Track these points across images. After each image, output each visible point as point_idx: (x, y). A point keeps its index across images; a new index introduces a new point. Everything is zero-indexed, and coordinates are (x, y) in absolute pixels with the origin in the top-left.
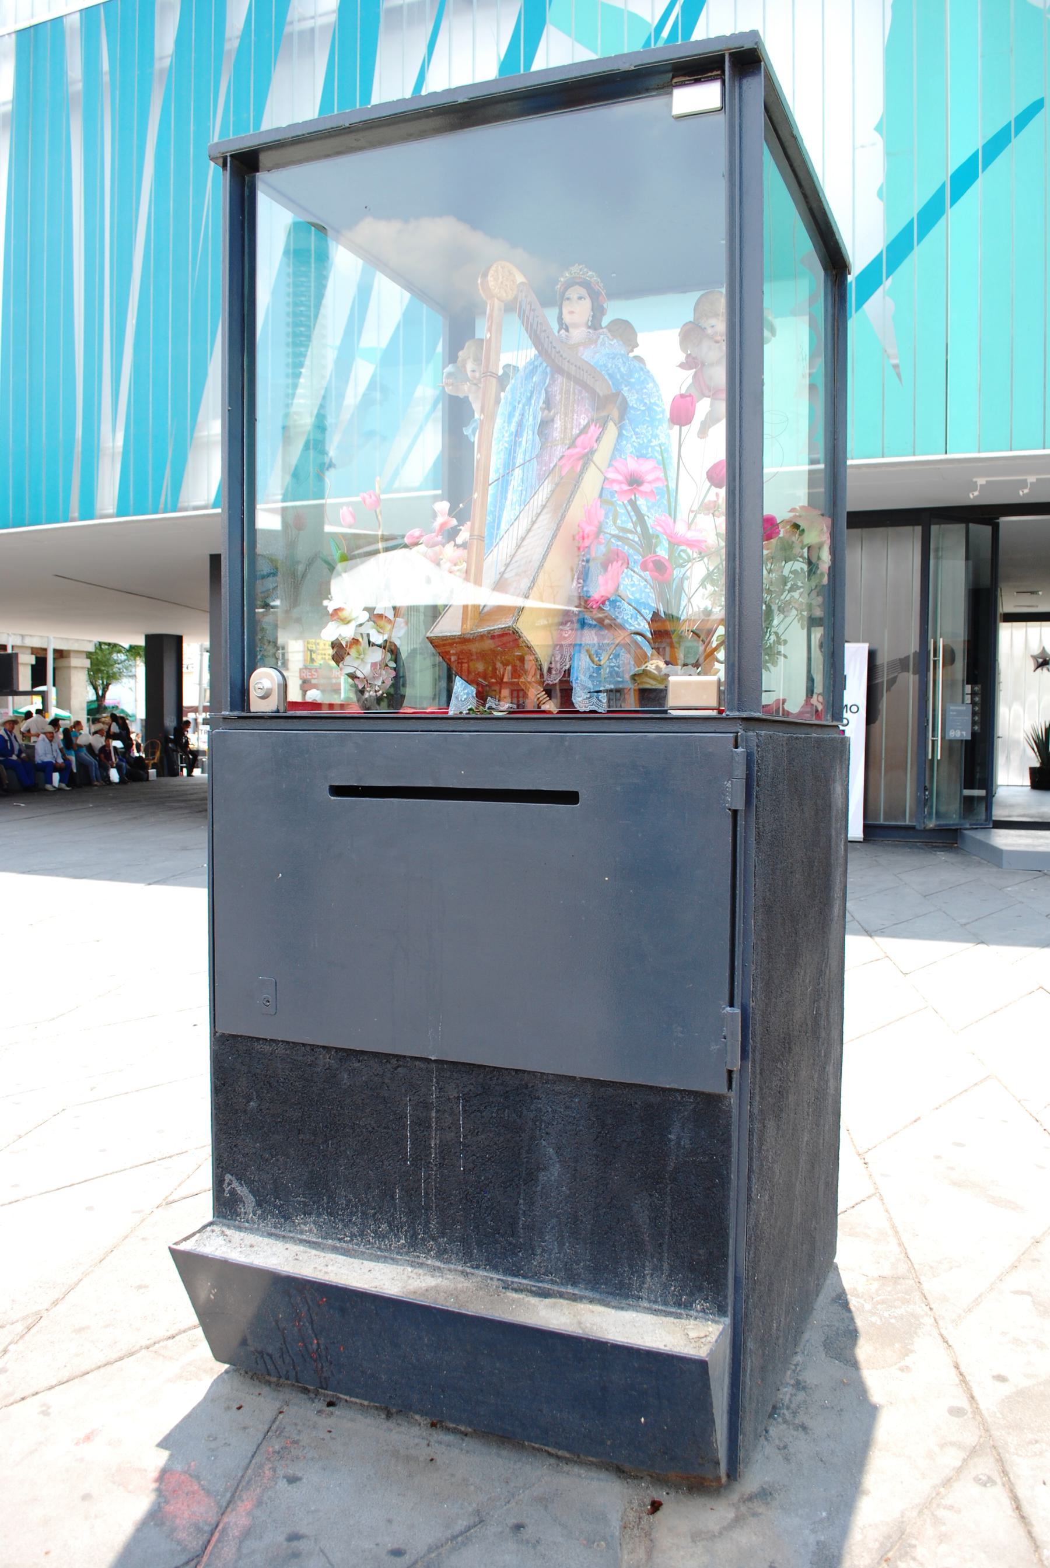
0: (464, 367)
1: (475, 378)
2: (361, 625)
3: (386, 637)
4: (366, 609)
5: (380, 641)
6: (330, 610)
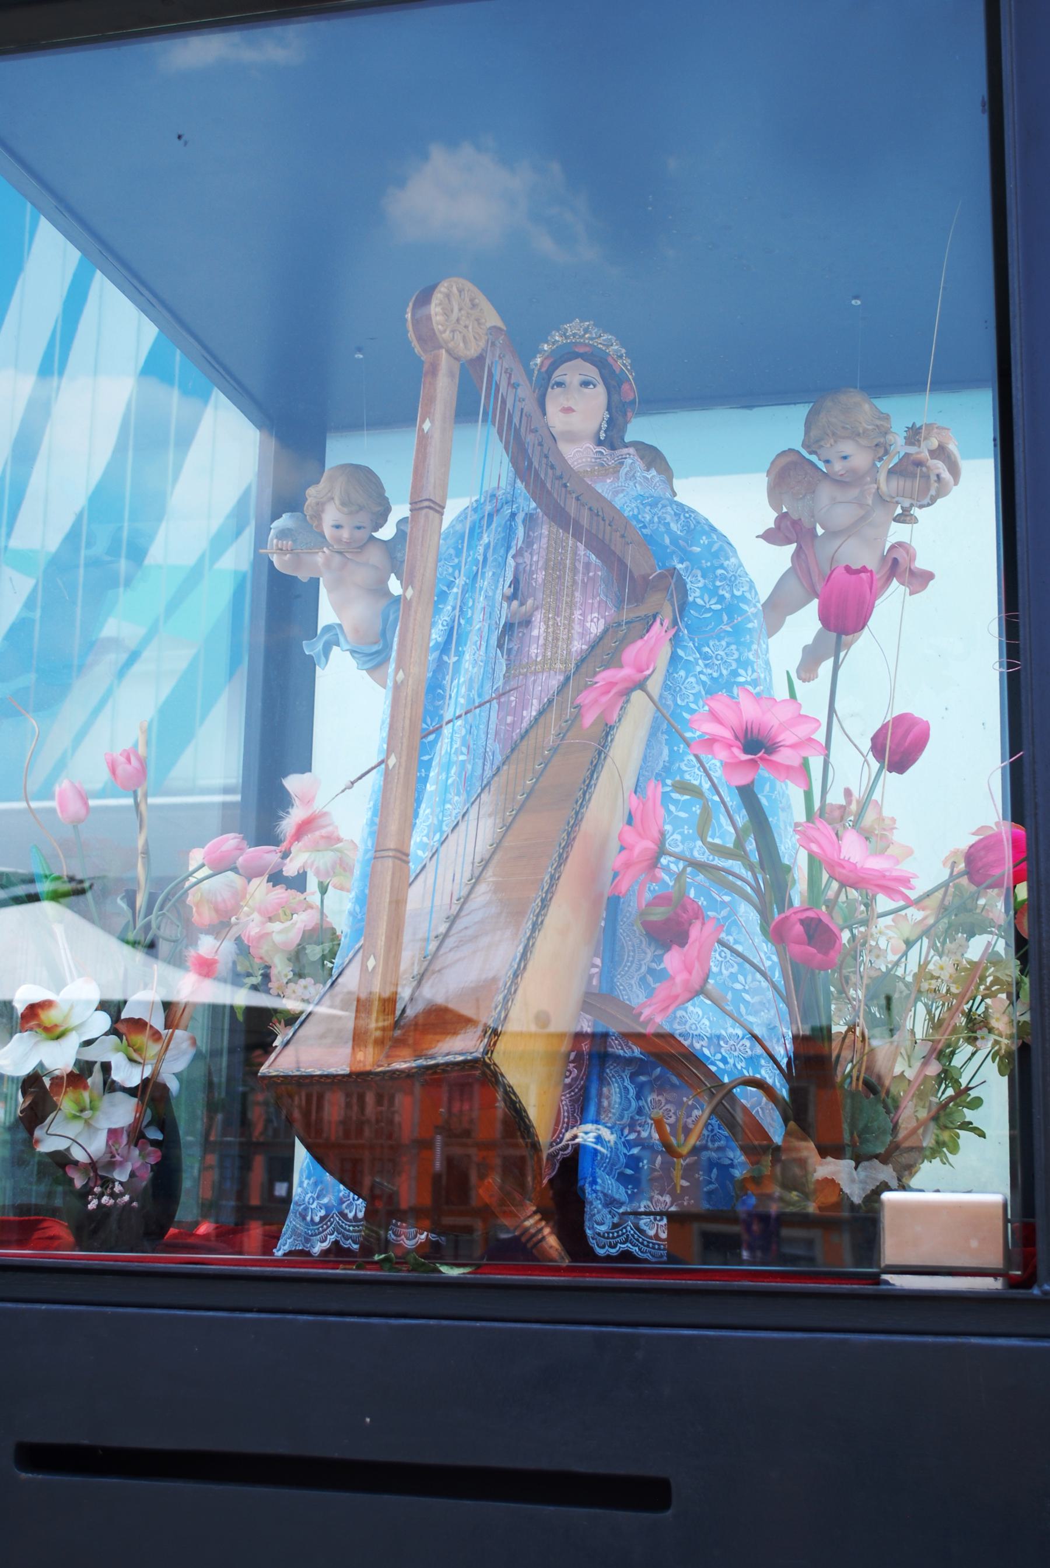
0: (318, 516)
1: (339, 541)
2: (88, 1043)
3: (147, 1073)
4: (104, 1006)
5: (134, 1081)
6: (20, 1008)
